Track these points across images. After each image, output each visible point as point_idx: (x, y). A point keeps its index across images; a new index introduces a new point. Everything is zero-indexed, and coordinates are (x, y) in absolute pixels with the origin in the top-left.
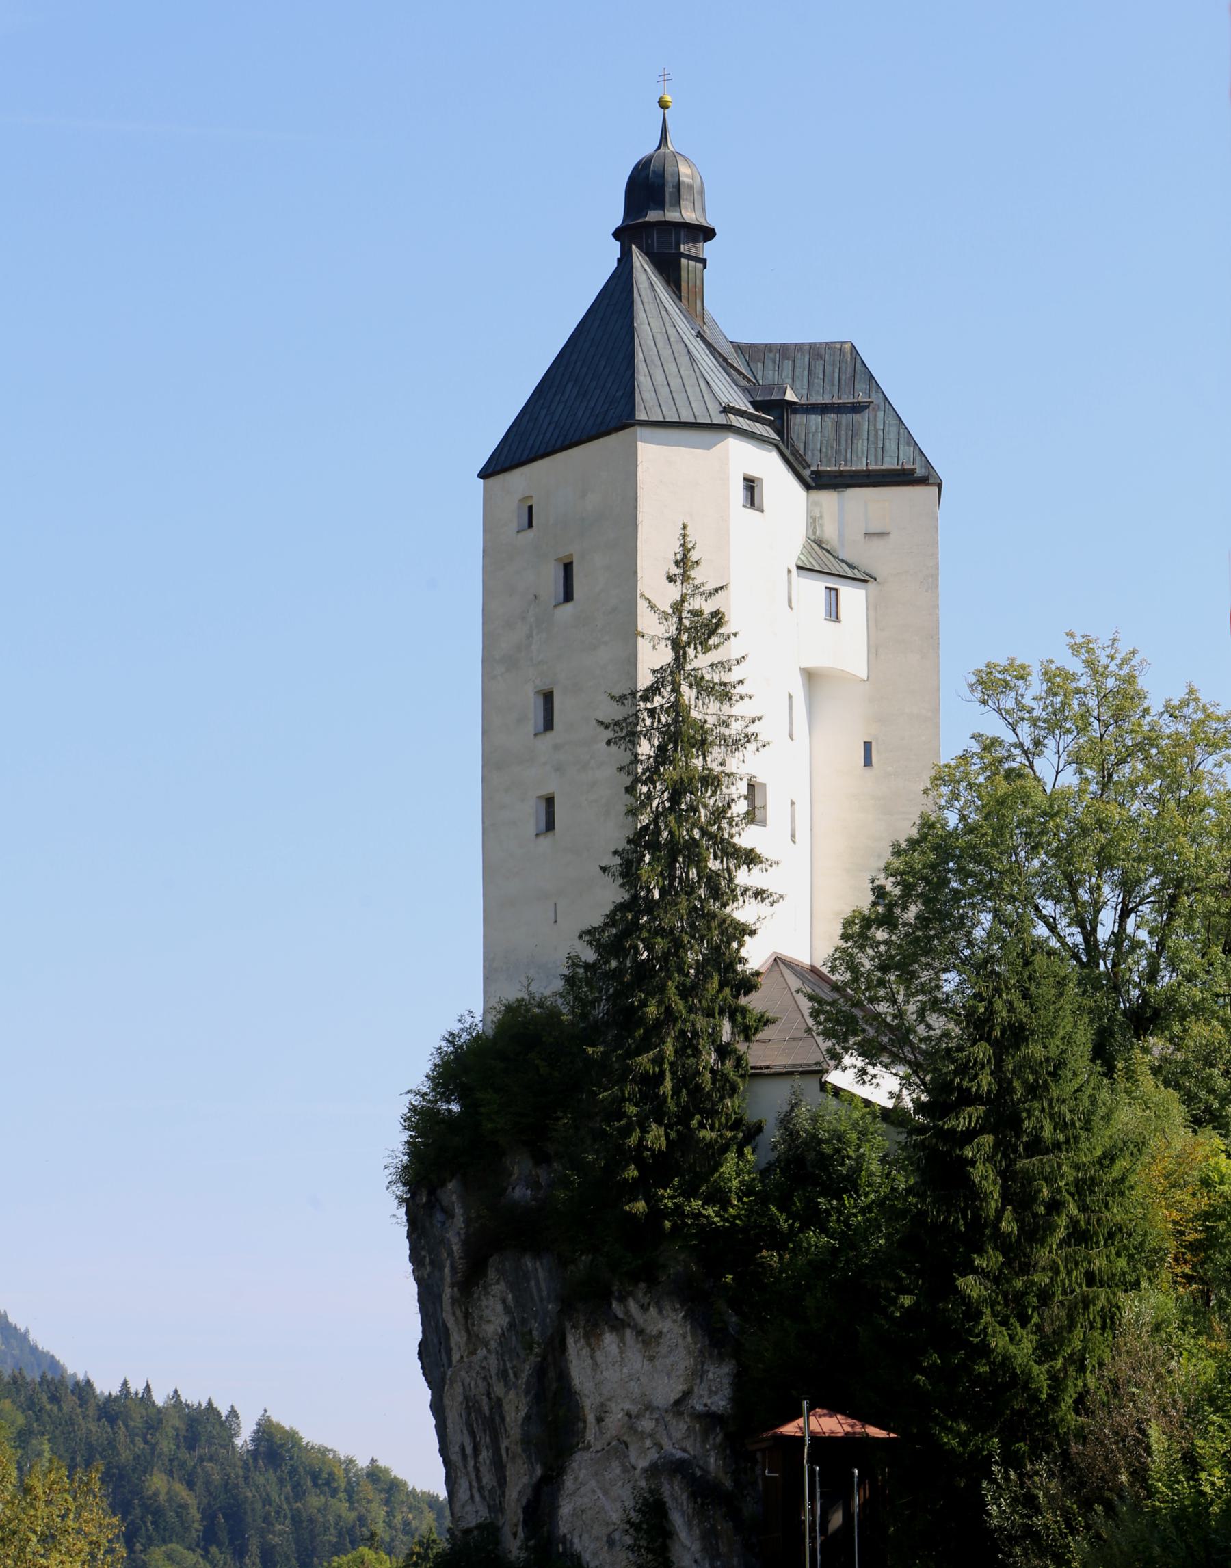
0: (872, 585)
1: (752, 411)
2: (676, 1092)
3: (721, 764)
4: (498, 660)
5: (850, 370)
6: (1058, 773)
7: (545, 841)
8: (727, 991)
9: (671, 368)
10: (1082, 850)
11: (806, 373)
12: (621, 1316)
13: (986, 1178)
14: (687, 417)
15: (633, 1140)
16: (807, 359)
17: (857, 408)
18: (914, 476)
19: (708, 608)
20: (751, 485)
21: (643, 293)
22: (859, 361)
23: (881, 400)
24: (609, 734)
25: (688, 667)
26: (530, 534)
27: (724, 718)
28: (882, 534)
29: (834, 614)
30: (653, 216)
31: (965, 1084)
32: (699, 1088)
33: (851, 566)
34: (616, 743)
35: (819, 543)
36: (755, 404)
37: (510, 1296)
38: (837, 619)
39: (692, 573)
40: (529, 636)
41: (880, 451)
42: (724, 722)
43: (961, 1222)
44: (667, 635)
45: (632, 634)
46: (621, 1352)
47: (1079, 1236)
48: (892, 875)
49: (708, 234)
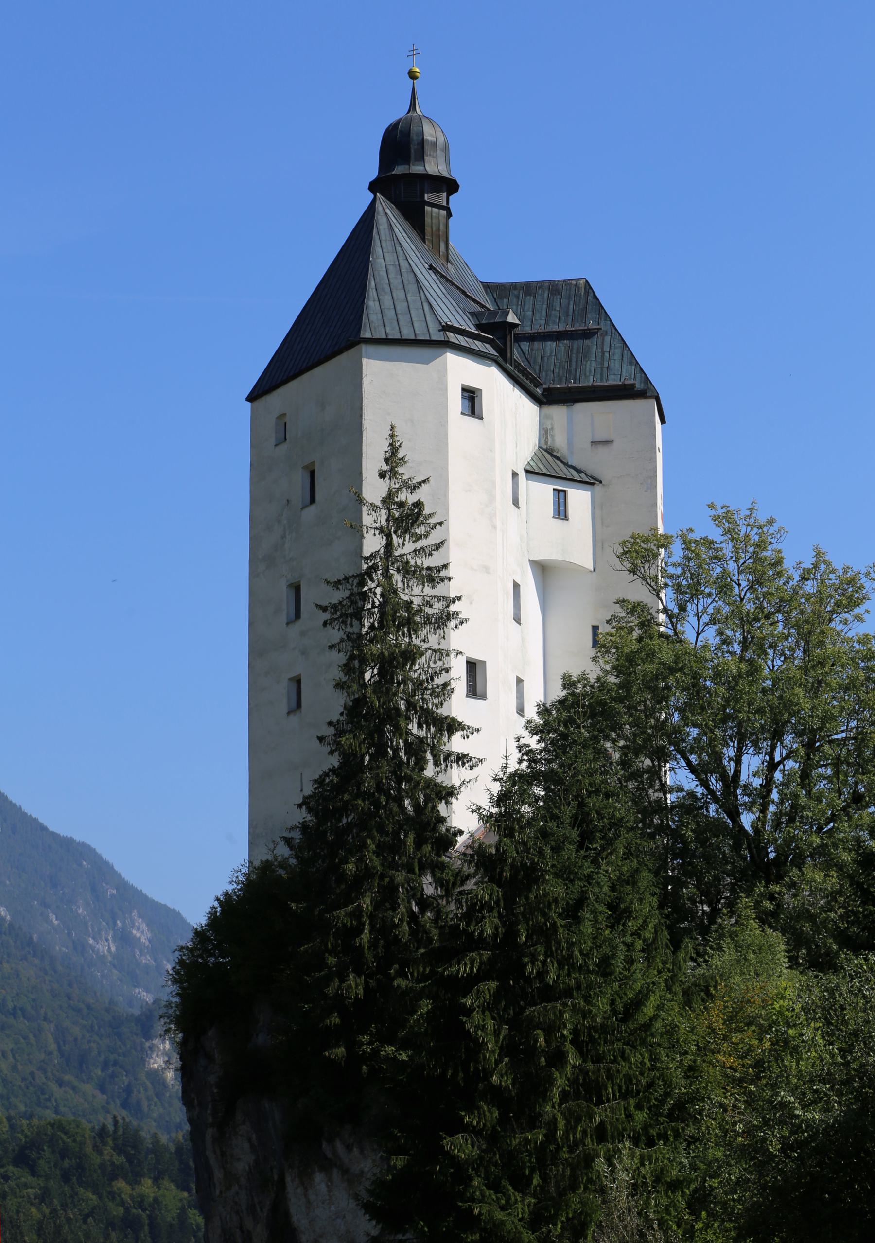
0: (598, 488)
1: (474, 330)
2: (373, 944)
3: (424, 641)
4: (261, 560)
5: (583, 302)
6: (698, 634)
7: (294, 719)
8: (427, 848)
9: (399, 294)
10: (740, 709)
11: (545, 306)
12: (330, 1156)
13: (483, 1028)
14: (408, 334)
15: (331, 990)
16: (546, 295)
17: (587, 334)
18: (636, 390)
19: (412, 499)
20: (471, 396)
21: (382, 232)
22: (591, 295)
23: (609, 327)
24: (327, 616)
25: (397, 553)
26: (284, 447)
27: (428, 599)
28: (607, 442)
29: (561, 511)
30: (399, 170)
31: (471, 929)
32: (397, 940)
33: (579, 471)
34: (331, 624)
35: (550, 452)
36: (478, 327)
37: (254, 1136)
38: (566, 518)
39: (400, 470)
40: (283, 537)
41: (605, 370)
42: (428, 602)
43: (461, 1075)
44: (375, 525)
45: (357, 530)
46: (329, 1191)
47: (588, 1089)
48: (536, 734)
49: (451, 186)
